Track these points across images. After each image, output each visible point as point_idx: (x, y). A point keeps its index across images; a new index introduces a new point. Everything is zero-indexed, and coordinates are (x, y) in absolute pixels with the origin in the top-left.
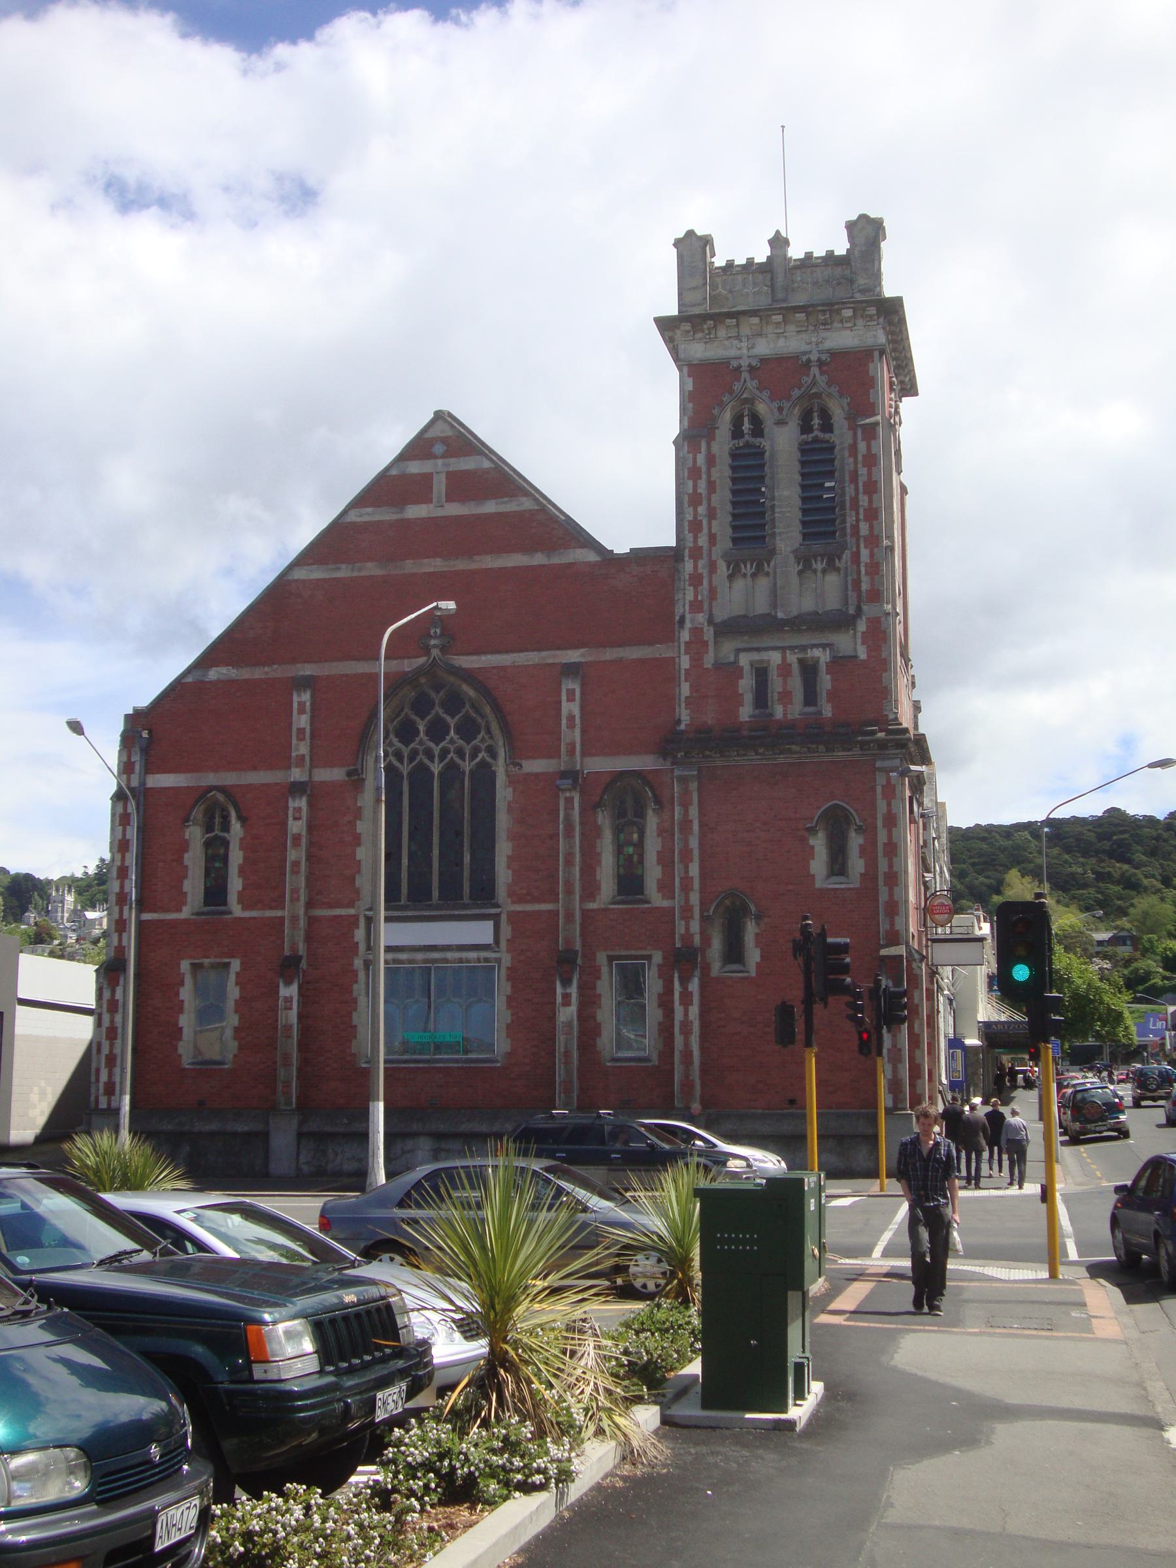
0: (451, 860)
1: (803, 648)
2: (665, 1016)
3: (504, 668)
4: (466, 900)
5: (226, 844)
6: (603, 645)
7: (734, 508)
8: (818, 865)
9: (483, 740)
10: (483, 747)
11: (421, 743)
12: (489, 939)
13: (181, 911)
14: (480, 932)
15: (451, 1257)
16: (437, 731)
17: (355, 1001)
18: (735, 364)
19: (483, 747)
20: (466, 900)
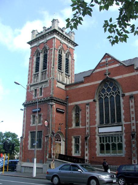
0: (113, 116)
4: (110, 123)
5: (79, 114)
9: (117, 90)
10: (117, 92)
11: (111, 92)
12: (120, 130)
13: (95, 125)
14: (119, 129)
16: (109, 89)
19: (117, 92)
20: (110, 123)
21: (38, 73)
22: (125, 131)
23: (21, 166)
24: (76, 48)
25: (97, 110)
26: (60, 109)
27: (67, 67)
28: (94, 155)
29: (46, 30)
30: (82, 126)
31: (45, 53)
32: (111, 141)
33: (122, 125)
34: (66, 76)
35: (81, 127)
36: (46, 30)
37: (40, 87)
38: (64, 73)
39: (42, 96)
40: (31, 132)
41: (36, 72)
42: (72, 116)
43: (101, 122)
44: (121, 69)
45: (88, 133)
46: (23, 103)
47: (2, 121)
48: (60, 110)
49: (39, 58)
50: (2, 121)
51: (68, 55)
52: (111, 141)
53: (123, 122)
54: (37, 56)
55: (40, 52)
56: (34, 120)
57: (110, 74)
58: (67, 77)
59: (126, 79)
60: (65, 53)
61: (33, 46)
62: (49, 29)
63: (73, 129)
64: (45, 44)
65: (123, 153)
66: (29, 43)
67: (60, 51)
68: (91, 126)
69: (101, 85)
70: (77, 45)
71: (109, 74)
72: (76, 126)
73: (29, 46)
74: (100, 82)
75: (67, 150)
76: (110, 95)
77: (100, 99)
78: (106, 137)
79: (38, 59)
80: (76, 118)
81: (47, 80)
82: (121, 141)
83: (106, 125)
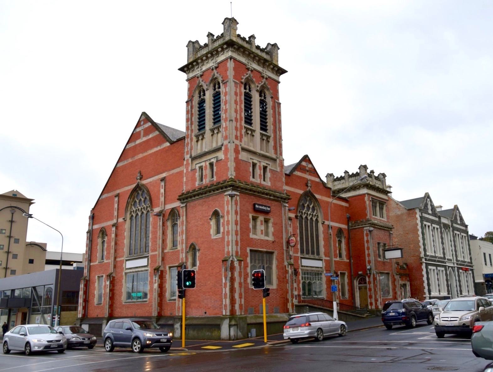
1: (210, 160)
2: (160, 291)
3: (151, 182)
6: (170, 170)
7: (199, 116)
8: (213, 231)
13: (298, 254)
15: (397, 361)
17: (123, 285)
18: (197, 76)
21: (204, 133)
23: (248, 324)
24: (282, 78)
26: (262, 205)
29: (214, 41)
33: (147, 257)
36: (214, 41)
38: (258, 131)
41: (199, 130)
42: (365, 202)
46: (179, 196)
48: (260, 207)
49: (220, 94)
55: (205, 87)
56: (255, 227)
58: (265, 139)
61: (191, 75)
62: (218, 38)
63: (249, 247)
64: (215, 70)
65: (176, 296)
66: (182, 69)
69: (133, 197)
70: (283, 71)
73: (184, 76)
79: (202, 102)
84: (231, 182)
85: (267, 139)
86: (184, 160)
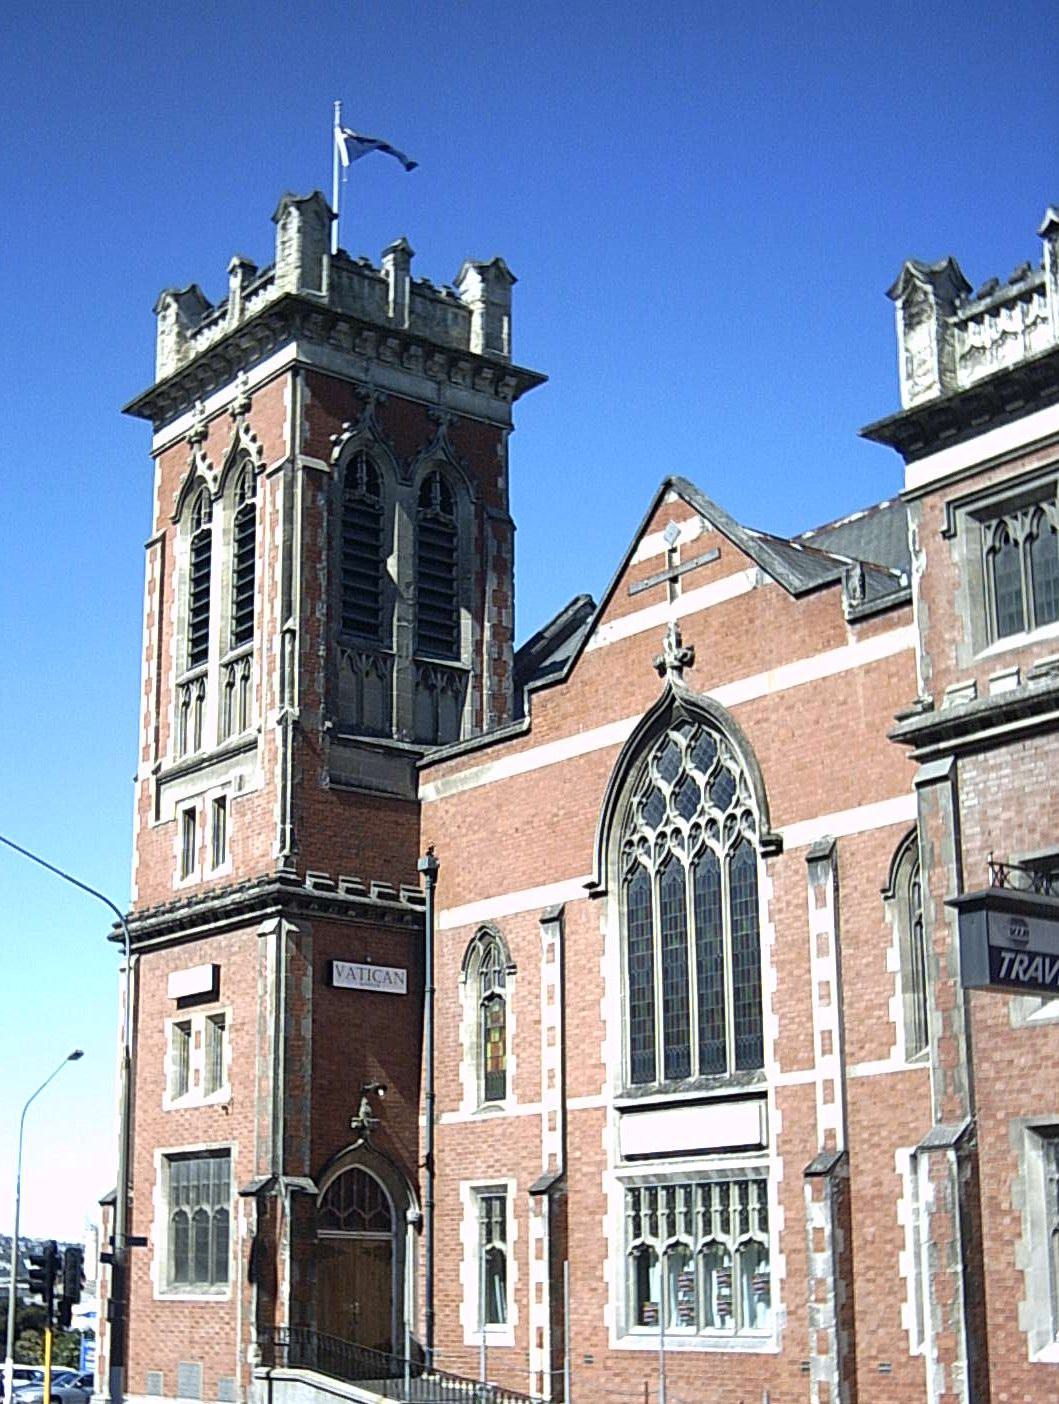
13: (599, 1091)
21: (205, 675)
22: (784, 1140)
25: (613, 968)
27: (435, 579)
28: (595, 1340)
30: (523, 1099)
31: (242, 497)
32: (735, 1221)
34: (426, 677)
35: (511, 1106)
37: (218, 793)
39: (226, 868)
40: (170, 1157)
43: (641, 1070)
44: (758, 622)
45: (830, 1135)
47: (77, 1055)
50: (77, 1055)
51: (445, 491)
52: (735, 1221)
53: (773, 1075)
54: (242, 497)
57: (690, 663)
59: (790, 708)
60: (407, 480)
67: (362, 474)
68: (857, 1071)
71: (685, 662)
72: (487, 1099)
74: (622, 730)
75: (435, 1301)
76: (693, 837)
77: (631, 871)
78: (706, 1188)
79: (202, 546)
80: (488, 1032)
81: (252, 738)
82: (764, 1225)
83: (708, 1088)
84: (277, 886)
85: (451, 680)
86: (136, 779)
